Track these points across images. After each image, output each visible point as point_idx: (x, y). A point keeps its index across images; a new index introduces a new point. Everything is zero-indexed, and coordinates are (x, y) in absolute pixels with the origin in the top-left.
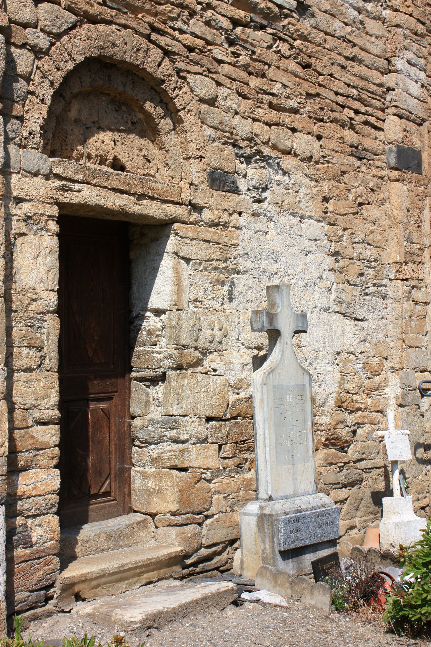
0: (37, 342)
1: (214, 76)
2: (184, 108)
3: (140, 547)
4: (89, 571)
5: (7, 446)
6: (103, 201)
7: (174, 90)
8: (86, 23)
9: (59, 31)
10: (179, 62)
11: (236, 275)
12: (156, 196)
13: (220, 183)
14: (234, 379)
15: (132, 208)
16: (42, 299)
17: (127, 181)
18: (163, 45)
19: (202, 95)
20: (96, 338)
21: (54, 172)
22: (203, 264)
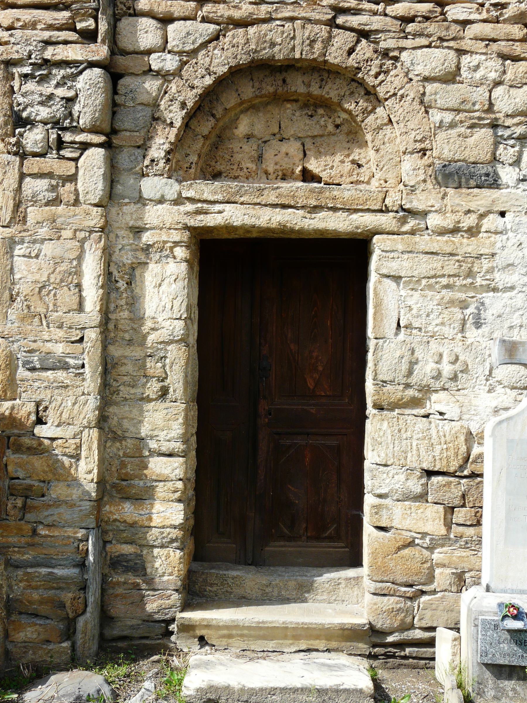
0: (157, 372)
1: (452, 44)
2: (395, 94)
3: (340, 607)
4: (269, 619)
5: (96, 474)
6: (253, 220)
7: (376, 76)
8: (232, 29)
9: (192, 47)
10: (385, 40)
11: (491, 294)
12: (339, 206)
13: (460, 178)
14: (477, 427)
15: (299, 224)
16: (163, 328)
17: (292, 193)
18: (357, 27)
19: (427, 74)
20: (320, 368)
21: (184, 196)
22: (424, 282)
